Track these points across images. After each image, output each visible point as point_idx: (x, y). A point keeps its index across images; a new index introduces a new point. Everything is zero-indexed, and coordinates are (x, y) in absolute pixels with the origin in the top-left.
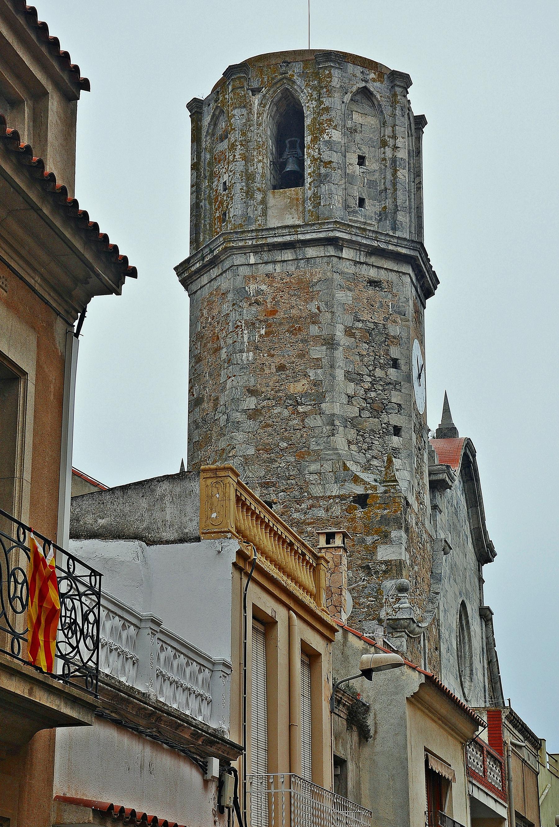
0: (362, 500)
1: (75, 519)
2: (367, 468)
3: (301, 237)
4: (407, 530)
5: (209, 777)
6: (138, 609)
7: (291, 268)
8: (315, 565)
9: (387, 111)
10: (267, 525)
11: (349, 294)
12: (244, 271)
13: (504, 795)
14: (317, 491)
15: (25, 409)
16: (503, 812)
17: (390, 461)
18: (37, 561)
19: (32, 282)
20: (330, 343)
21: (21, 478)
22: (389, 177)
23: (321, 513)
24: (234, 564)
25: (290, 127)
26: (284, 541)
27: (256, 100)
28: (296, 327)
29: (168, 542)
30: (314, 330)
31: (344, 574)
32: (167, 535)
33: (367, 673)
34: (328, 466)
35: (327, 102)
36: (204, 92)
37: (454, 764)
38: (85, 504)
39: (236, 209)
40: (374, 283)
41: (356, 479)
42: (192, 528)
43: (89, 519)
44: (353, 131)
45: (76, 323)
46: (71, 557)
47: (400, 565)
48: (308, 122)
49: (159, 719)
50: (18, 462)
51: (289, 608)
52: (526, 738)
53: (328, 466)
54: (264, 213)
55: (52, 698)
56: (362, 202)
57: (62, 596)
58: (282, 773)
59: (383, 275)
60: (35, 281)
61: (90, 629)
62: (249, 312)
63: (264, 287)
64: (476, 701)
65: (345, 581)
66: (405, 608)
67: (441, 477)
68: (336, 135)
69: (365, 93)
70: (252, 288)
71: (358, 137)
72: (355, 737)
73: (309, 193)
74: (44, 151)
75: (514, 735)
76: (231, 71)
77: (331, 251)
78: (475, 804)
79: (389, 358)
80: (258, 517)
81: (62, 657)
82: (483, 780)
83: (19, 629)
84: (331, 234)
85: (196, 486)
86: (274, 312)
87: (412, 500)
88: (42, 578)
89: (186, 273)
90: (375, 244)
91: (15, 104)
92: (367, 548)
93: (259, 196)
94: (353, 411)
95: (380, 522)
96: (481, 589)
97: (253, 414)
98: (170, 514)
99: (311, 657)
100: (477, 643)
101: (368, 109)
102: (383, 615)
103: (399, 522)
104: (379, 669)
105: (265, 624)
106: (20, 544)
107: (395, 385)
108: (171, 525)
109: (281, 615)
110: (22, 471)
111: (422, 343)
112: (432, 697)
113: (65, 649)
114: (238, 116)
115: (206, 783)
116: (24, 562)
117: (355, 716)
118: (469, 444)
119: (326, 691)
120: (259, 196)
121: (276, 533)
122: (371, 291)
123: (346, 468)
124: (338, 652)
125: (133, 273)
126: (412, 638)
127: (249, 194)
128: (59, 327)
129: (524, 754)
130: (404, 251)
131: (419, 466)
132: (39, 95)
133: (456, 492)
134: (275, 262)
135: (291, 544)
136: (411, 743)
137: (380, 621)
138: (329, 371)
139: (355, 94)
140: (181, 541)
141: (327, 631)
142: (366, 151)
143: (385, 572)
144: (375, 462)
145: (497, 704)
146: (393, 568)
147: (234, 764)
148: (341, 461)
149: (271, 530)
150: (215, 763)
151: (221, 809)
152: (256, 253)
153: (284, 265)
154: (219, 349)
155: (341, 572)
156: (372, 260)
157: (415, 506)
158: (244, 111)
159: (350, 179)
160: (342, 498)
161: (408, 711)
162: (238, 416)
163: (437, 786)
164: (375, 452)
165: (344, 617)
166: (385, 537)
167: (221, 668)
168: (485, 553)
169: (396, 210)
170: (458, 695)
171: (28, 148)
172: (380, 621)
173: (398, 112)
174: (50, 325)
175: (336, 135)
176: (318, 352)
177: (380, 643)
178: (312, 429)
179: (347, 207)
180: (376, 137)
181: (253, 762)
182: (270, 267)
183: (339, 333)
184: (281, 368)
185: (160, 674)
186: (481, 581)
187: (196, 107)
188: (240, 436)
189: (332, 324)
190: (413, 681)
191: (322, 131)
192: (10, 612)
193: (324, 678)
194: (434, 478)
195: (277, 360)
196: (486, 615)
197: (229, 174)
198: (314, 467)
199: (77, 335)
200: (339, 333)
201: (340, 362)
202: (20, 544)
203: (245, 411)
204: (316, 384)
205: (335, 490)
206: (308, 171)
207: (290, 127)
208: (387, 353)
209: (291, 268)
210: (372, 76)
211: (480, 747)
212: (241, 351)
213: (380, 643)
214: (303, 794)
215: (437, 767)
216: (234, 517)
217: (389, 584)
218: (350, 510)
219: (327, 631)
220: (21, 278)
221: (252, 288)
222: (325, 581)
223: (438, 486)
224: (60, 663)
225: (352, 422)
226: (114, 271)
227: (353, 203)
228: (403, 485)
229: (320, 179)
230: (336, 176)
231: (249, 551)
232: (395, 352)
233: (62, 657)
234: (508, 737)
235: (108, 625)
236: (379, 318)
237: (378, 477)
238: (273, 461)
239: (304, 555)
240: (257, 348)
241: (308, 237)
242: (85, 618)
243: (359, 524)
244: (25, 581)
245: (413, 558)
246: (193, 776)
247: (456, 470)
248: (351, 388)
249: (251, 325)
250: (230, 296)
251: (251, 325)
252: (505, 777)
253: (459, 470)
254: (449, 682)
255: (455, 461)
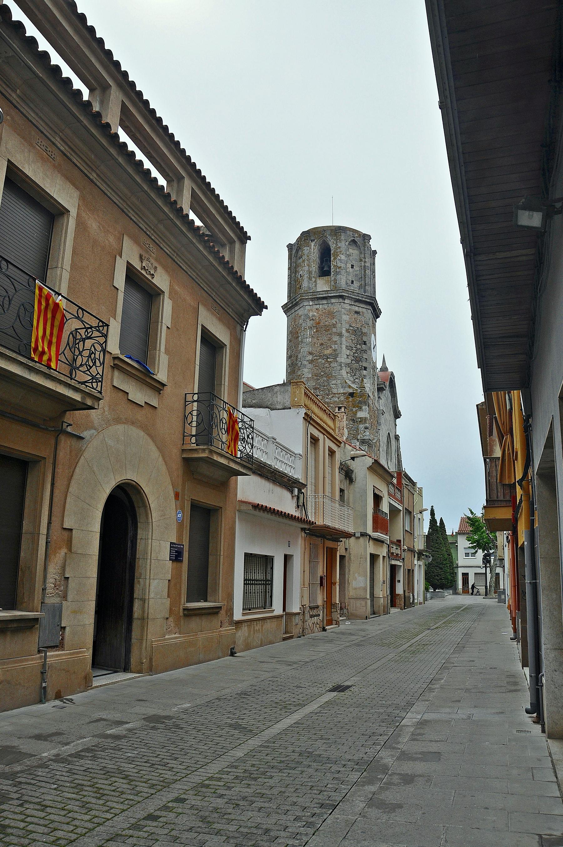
0: (352, 395)
1: (244, 400)
2: (354, 382)
3: (330, 295)
4: (368, 406)
5: (294, 495)
6: (267, 434)
7: (326, 307)
8: (334, 418)
9: (362, 248)
10: (316, 403)
11: (348, 316)
12: (308, 308)
13: (401, 502)
14: (335, 391)
15: (225, 361)
16: (401, 508)
17: (362, 380)
18: (231, 415)
19: (228, 311)
20: (340, 335)
21: (224, 384)
22: (363, 273)
23: (337, 399)
24: (304, 418)
25: (326, 254)
26: (322, 409)
27: (313, 244)
28: (327, 328)
29: (279, 409)
30: (334, 330)
31: (345, 422)
32: (278, 407)
33: (353, 459)
34: (339, 382)
35: (339, 245)
36: (293, 241)
37: (384, 491)
38: (248, 395)
39: (305, 284)
40: (357, 313)
41: (350, 387)
42: (288, 404)
43: (249, 400)
44: (349, 255)
45: (245, 327)
46: (243, 414)
47: (366, 419)
48: (332, 252)
49: (275, 474)
50: (223, 378)
51: (324, 434)
52: (410, 482)
53: (339, 382)
54: (316, 286)
55: (236, 465)
56: (352, 282)
57: (240, 428)
58: (321, 493)
59: (360, 310)
60: (230, 311)
61: (250, 441)
62: (309, 323)
63: (315, 314)
64: (392, 468)
65: (345, 425)
66: (367, 435)
67: (381, 386)
68: (343, 257)
69: (354, 242)
70: (311, 314)
71: (351, 258)
72: (348, 482)
73: (333, 278)
74: (234, 262)
75: (406, 481)
76: (303, 233)
77: (341, 300)
78: (390, 505)
79: (362, 342)
80: (313, 400)
81: (240, 450)
82: (394, 497)
83: (224, 440)
84: (341, 294)
85: (289, 388)
86: (319, 323)
87: (370, 395)
88: (233, 422)
89: (287, 309)
90: (358, 298)
91: (223, 245)
92: (353, 413)
93: (314, 279)
94: (349, 361)
95: (358, 403)
96: (395, 428)
97: (311, 362)
98: (280, 398)
99: (332, 453)
100: (394, 448)
101: (355, 248)
102: (359, 437)
103: (366, 403)
104: (357, 457)
105: (315, 440)
106: (224, 409)
107: (365, 351)
108: (280, 403)
109: (321, 437)
110: (224, 382)
111: (375, 335)
112: (377, 468)
113: (241, 448)
114: (306, 250)
115: (293, 497)
116: (225, 415)
117: (348, 474)
118: (392, 374)
119: (337, 465)
120: (314, 279)
121: (319, 406)
122: (356, 315)
123: (346, 382)
124: (342, 451)
125: (266, 307)
126: (370, 446)
127: (310, 279)
128: (238, 327)
129: (409, 488)
130: (368, 301)
131: (374, 382)
132: (232, 242)
133: (387, 392)
134: (319, 304)
135: (325, 411)
136: (367, 483)
137: (358, 440)
138: (340, 345)
139: (350, 242)
140: (284, 409)
141: (338, 443)
142: (354, 263)
143: (360, 422)
144: (357, 380)
145: (400, 470)
146: (363, 420)
147: (303, 491)
148: (343, 380)
149: (318, 405)
150: (296, 490)
151: (298, 506)
152: (312, 301)
153: (323, 306)
154: (298, 337)
155: (343, 421)
156: (357, 304)
157: (372, 397)
158: (308, 248)
159: (348, 273)
160: (344, 394)
161: (368, 472)
162: (305, 363)
163: (377, 499)
164: (357, 377)
165: (345, 438)
166: (360, 408)
167: (298, 456)
168: (397, 415)
169: (365, 285)
170: (386, 467)
171: (228, 261)
172: (358, 440)
173: (366, 249)
174: (235, 328)
175: (343, 257)
176: (336, 338)
177: (358, 448)
178: (333, 367)
179: (347, 284)
180: (358, 258)
181: (309, 491)
182: (318, 306)
183: (344, 331)
184: (322, 344)
185: (276, 458)
186: (396, 425)
187: (290, 247)
188: (306, 370)
189: (341, 328)
190: (369, 461)
191: (338, 255)
192: (221, 434)
193: (337, 460)
194: (379, 386)
195: (321, 341)
196: (397, 438)
197: (303, 271)
198: (334, 382)
199: (245, 331)
200: (344, 331)
201: (344, 342)
202: (224, 409)
203: (308, 360)
204: (335, 350)
205: (342, 391)
206: (332, 270)
207: (326, 254)
208: (362, 339)
209: (326, 307)
210: (356, 235)
211: (393, 485)
212: (307, 338)
213: (358, 448)
214: (327, 501)
215: (376, 491)
216: (303, 400)
217: (361, 426)
218: (347, 398)
219: (338, 443)
220: (224, 310)
221: (311, 314)
222: (337, 425)
223: (380, 390)
224: (239, 453)
225: (348, 365)
226: (258, 307)
227: (350, 282)
228: (367, 389)
229: (337, 273)
230: (343, 272)
231: (309, 413)
232: (365, 339)
233: (240, 450)
234: (404, 482)
235: (257, 439)
236: (359, 326)
237: (358, 386)
238: (318, 379)
239: (330, 414)
240: (312, 337)
241: (332, 295)
242: (248, 437)
243: (351, 403)
244: (226, 422)
245: (371, 416)
246: (287, 495)
247: (387, 384)
248: (348, 352)
249: (310, 328)
250: (302, 317)
251: (310, 328)
252: (402, 496)
253: (388, 385)
254: (383, 462)
255: (387, 380)
